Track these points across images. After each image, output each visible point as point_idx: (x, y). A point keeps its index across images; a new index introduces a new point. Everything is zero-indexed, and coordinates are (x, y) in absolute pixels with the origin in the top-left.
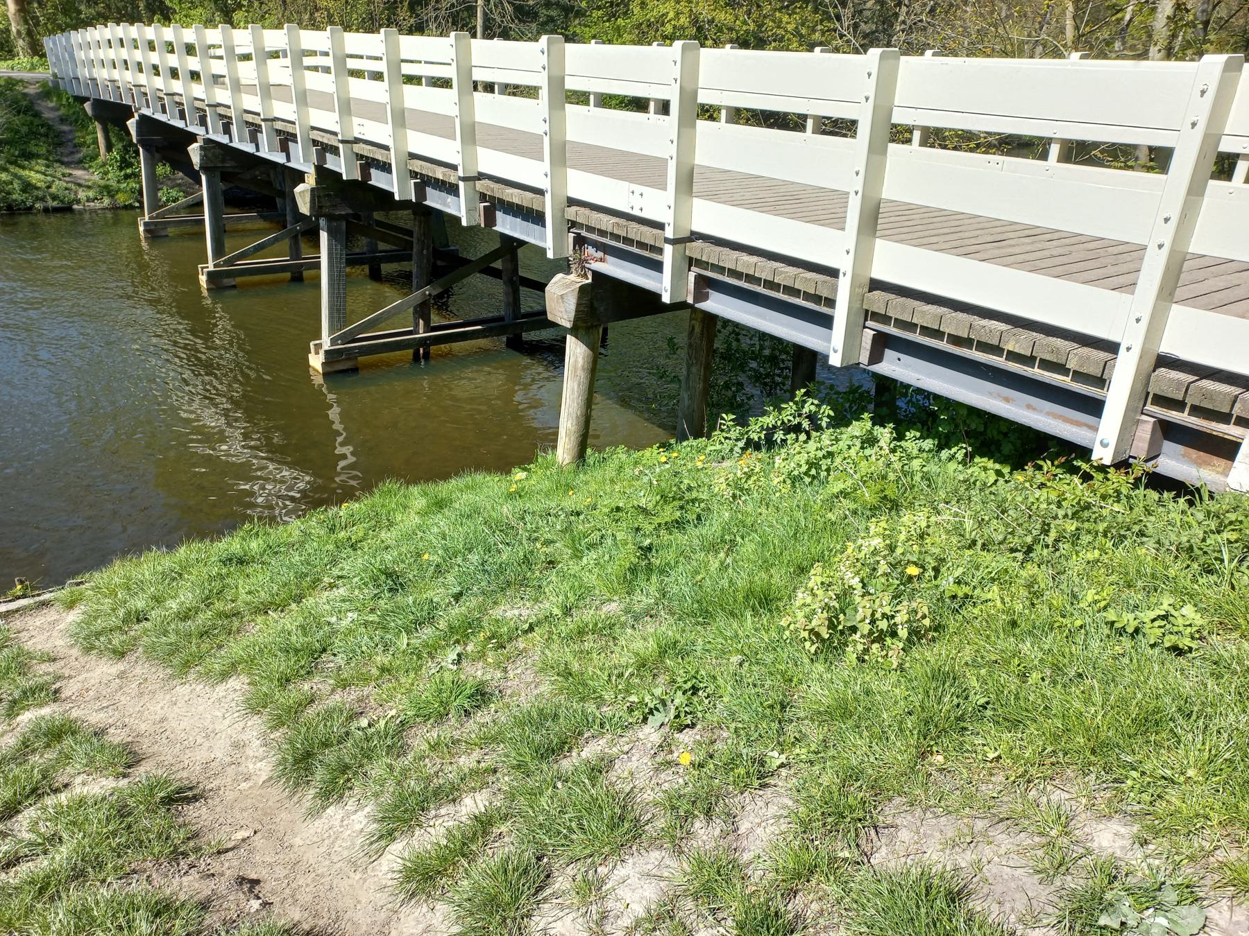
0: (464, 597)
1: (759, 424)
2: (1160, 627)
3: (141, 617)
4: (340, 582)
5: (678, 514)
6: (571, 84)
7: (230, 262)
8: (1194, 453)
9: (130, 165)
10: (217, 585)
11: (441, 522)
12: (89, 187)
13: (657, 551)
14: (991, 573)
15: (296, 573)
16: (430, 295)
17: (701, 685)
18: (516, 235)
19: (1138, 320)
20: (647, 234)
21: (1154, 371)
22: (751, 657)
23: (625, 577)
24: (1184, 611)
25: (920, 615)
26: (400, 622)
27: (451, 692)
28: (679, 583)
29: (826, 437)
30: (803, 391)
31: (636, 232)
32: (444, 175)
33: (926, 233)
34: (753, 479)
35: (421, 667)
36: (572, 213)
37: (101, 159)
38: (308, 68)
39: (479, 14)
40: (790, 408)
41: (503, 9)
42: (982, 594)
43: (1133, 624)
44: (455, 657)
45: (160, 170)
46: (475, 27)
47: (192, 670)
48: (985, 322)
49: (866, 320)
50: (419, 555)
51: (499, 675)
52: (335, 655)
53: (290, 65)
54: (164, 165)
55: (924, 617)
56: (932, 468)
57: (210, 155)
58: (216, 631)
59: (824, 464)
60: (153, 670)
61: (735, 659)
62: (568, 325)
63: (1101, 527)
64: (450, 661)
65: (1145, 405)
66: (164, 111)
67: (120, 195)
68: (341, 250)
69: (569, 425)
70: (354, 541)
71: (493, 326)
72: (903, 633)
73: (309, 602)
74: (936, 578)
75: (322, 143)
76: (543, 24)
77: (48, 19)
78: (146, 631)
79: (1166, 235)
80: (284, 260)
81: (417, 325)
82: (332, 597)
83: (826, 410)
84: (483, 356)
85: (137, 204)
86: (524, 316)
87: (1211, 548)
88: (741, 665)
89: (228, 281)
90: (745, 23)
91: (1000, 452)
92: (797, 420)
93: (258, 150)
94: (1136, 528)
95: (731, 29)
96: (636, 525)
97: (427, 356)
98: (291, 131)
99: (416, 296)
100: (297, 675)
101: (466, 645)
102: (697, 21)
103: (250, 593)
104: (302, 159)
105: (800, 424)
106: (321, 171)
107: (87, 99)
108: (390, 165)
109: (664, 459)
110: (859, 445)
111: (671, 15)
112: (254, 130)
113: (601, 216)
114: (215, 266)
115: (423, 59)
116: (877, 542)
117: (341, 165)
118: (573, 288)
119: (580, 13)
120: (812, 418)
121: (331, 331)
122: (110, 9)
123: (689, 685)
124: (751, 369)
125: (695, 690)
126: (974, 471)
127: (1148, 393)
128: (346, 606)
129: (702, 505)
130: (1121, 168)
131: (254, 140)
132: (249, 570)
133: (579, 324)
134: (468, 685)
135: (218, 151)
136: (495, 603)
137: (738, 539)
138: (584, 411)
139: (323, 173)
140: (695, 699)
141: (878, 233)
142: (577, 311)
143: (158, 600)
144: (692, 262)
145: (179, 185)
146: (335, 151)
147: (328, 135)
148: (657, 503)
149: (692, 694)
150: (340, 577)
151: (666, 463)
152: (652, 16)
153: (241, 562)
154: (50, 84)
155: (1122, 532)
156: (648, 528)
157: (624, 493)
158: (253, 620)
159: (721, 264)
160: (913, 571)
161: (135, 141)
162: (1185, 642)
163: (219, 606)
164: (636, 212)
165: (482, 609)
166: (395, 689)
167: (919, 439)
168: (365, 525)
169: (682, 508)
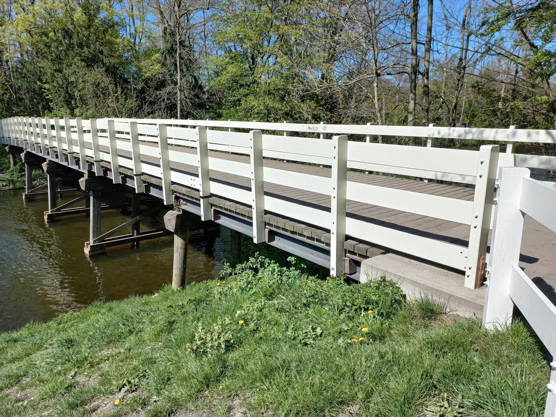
6: (350, 165)
7: (58, 210)
12: (4, 181)
18: (157, 196)
20: (193, 194)
36: (173, 187)
37: (11, 169)
38: (72, 132)
48: (299, 225)
49: (265, 225)
53: (131, 139)
57: (51, 167)
67: (18, 183)
69: (176, 272)
81: (133, 233)
89: (58, 218)
97: (138, 245)
107: (7, 145)
109: (218, 284)
111: (256, 105)
114: (51, 212)
115: (146, 134)
121: (94, 237)
133: (177, 230)
135: (55, 165)
138: (182, 266)
139: (91, 173)
142: (176, 225)
144: (212, 205)
164: (193, 187)
167: (295, 270)
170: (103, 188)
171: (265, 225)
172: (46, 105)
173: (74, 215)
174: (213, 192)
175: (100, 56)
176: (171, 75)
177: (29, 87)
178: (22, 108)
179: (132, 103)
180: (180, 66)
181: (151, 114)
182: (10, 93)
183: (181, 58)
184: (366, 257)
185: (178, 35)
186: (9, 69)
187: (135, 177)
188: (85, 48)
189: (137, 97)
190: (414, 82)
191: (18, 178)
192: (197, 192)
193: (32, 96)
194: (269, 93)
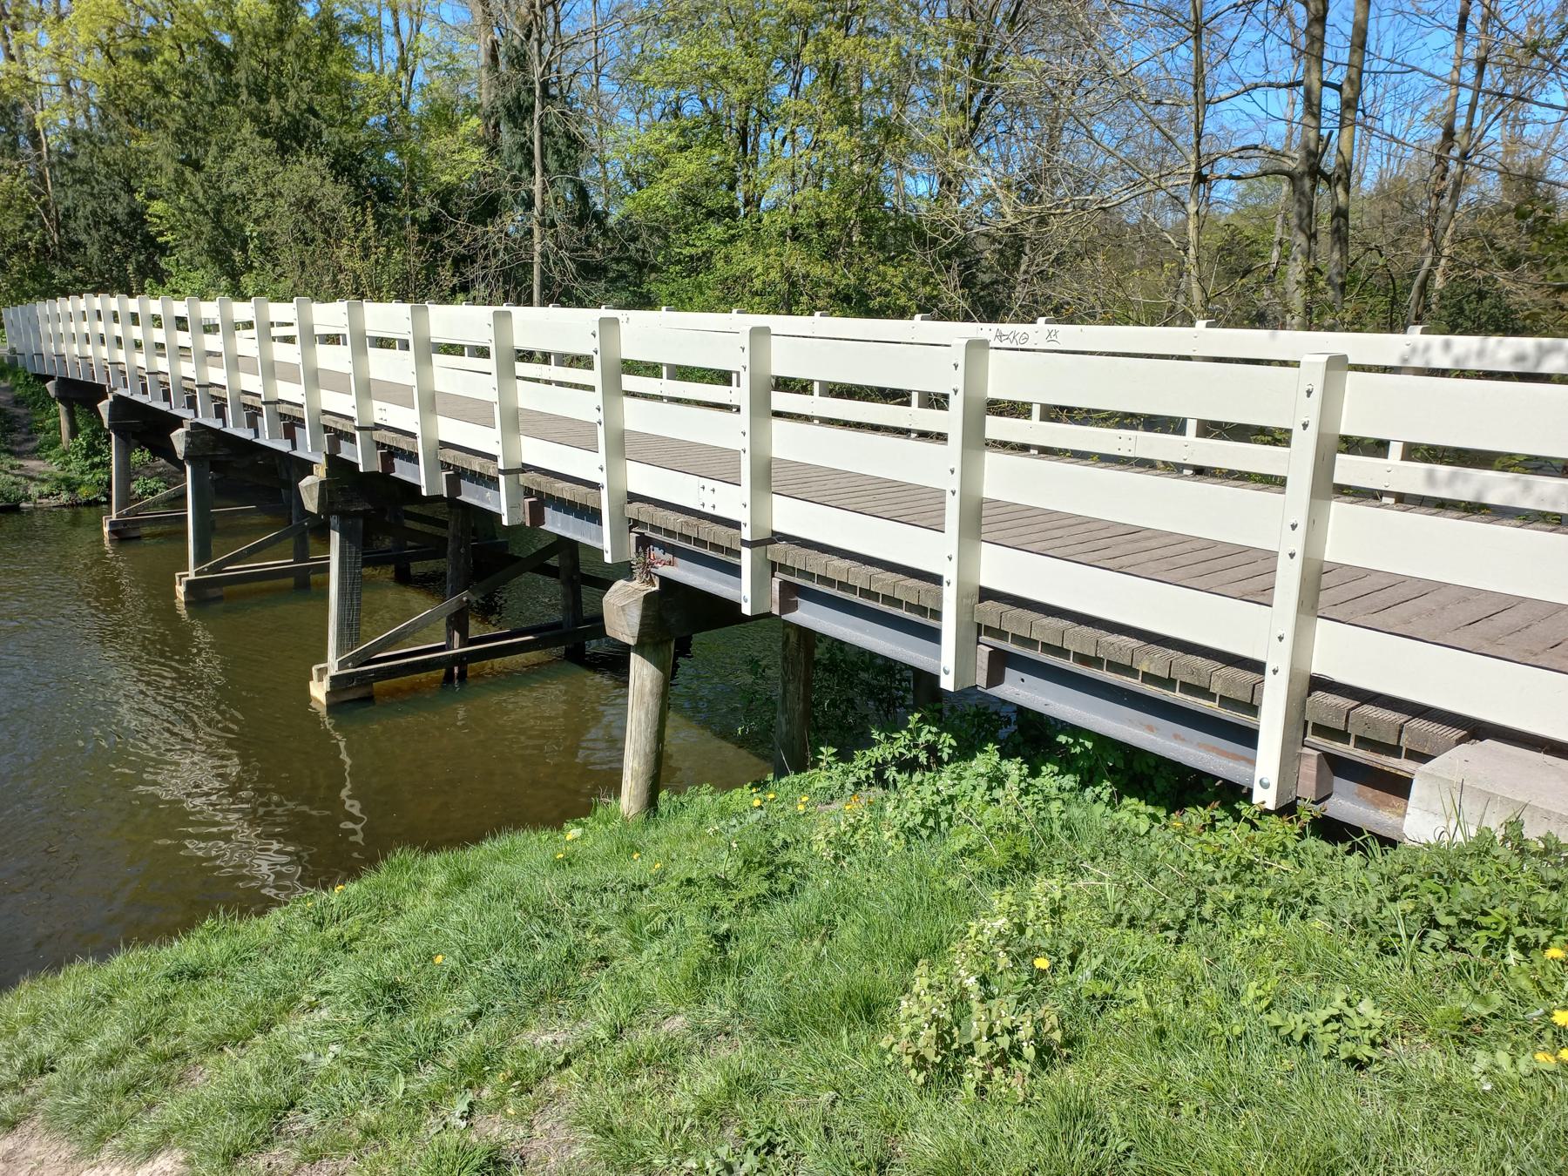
0: (483, 1018)
1: (866, 760)
2: (1334, 1031)
3: (45, 1067)
4: (323, 1001)
5: (766, 885)
7: (217, 568)
8: (1369, 792)
9: (99, 452)
10: (157, 1011)
11: (464, 907)
12: (44, 481)
13: (737, 939)
14: (1135, 962)
15: (266, 990)
16: (468, 601)
17: (779, 1139)
18: (568, 535)
19: (1281, 638)
20: (721, 535)
21: (1309, 695)
22: (846, 1093)
23: (695, 979)
24: (1362, 1007)
25: (1048, 1026)
26: (396, 1058)
27: (454, 1164)
28: (762, 986)
29: (945, 780)
30: (917, 716)
31: (708, 531)
32: (482, 466)
33: (1049, 525)
34: (860, 832)
35: (418, 1124)
36: (633, 510)
39: (536, 271)
40: (903, 737)
41: (565, 266)
42: (1126, 992)
43: (1302, 1029)
44: (465, 1108)
45: (136, 456)
46: (531, 286)
47: (108, 1146)
48: (1114, 638)
49: (979, 634)
50: (430, 957)
51: (522, 1133)
52: (305, 1112)
54: (143, 450)
55: (1053, 1029)
56: (1076, 812)
57: (198, 442)
58: (148, 1083)
59: (944, 811)
60: (55, 1147)
61: (827, 1096)
62: (632, 642)
63: (1266, 893)
64: (458, 1114)
65: (1305, 736)
66: (145, 392)
67: (82, 489)
68: (357, 553)
69: (636, 765)
70: (346, 939)
71: (546, 635)
72: (1029, 1052)
73: (280, 1031)
74: (1072, 969)
75: (335, 430)
76: (613, 281)
77: (12, 286)
78: (50, 1087)
79: (1296, 542)
80: (285, 562)
81: (451, 638)
82: (311, 1023)
83: (947, 739)
84: (534, 673)
85: (104, 499)
86: (587, 621)
87: (1387, 921)
88: (833, 1104)
89: (213, 592)
90: (844, 276)
91: (1154, 789)
92: (914, 752)
93: (257, 436)
94: (1307, 893)
95: (829, 284)
96: (712, 903)
97: (463, 676)
98: (298, 415)
99: (451, 604)
100: (251, 1145)
101: (482, 1089)
102: (790, 276)
103: (202, 1021)
104: (308, 447)
105: (916, 757)
106: (334, 462)
107: (51, 378)
108: (417, 454)
109: (757, 803)
110: (985, 785)
111: (759, 270)
112: (253, 415)
113: (668, 513)
114: (197, 573)
116: (1002, 922)
117: (357, 454)
118: (636, 597)
119: (654, 268)
120: (932, 749)
121: (340, 650)
122: (91, 273)
123: (763, 1140)
124: (862, 682)
125: (771, 1147)
126: (1124, 815)
127: (1306, 723)
128: (329, 1035)
129: (798, 870)
130: (1268, 443)
131: (253, 423)
132: (206, 987)
134: (477, 1154)
136: (524, 1025)
137: (839, 918)
138: (654, 746)
139: (336, 464)
140: (771, 1159)
141: (983, 537)
142: (642, 624)
143: (74, 1040)
144: (774, 567)
145: (160, 474)
146: (351, 438)
147: (344, 421)
148: (739, 871)
149: (767, 1154)
150: (324, 994)
151: (761, 808)
152: (737, 269)
153: (195, 975)
154: (6, 361)
155: (1291, 900)
156: (727, 907)
157: (697, 860)
158: (201, 1063)
159: (808, 570)
160: (1042, 963)
161: (106, 425)
162: (1364, 1052)
163: (156, 1044)
164: (708, 510)
165: (506, 1036)
166: (381, 1160)
167: (1058, 775)
168: (363, 915)
169: (770, 876)
170: (368, 507)
171: (979, 634)
172: (146, 263)
173: (254, 585)
174: (779, 526)
175: (313, 121)
176: (516, 180)
177: (99, 211)
178: (78, 272)
179: (407, 258)
180: (543, 155)
181: (462, 291)
182: (42, 225)
183: (545, 132)
184: (1424, 758)
185: (537, 62)
186: (40, 157)
187: (502, 478)
188: (273, 100)
189: (421, 242)
190: (1305, 201)
191: (83, 473)
192: (733, 531)
193: (107, 237)
194: (796, 235)
